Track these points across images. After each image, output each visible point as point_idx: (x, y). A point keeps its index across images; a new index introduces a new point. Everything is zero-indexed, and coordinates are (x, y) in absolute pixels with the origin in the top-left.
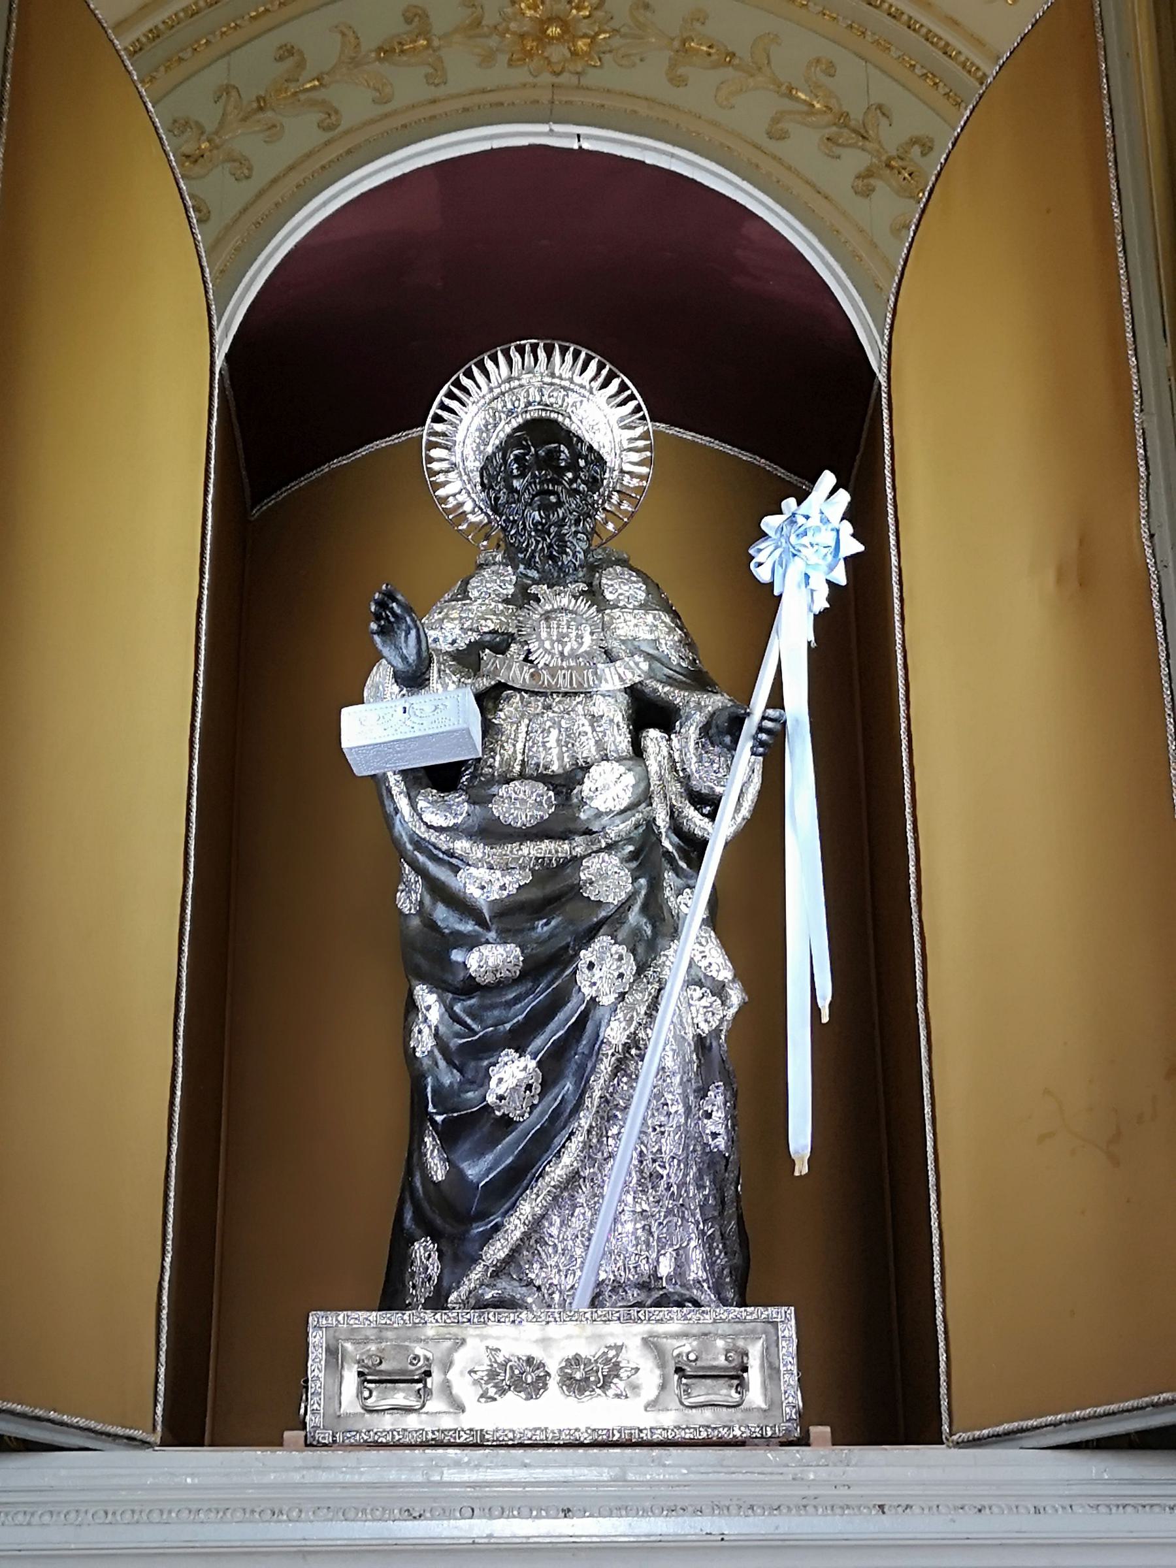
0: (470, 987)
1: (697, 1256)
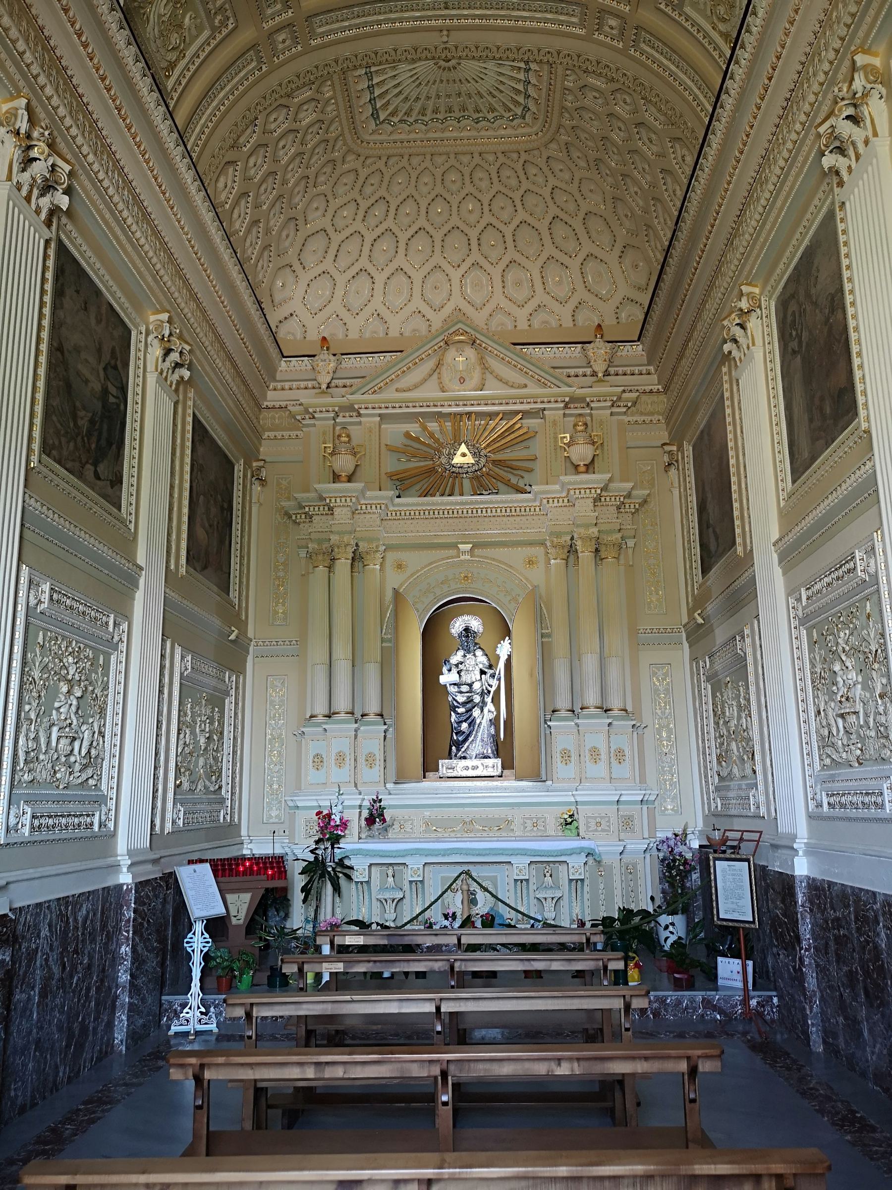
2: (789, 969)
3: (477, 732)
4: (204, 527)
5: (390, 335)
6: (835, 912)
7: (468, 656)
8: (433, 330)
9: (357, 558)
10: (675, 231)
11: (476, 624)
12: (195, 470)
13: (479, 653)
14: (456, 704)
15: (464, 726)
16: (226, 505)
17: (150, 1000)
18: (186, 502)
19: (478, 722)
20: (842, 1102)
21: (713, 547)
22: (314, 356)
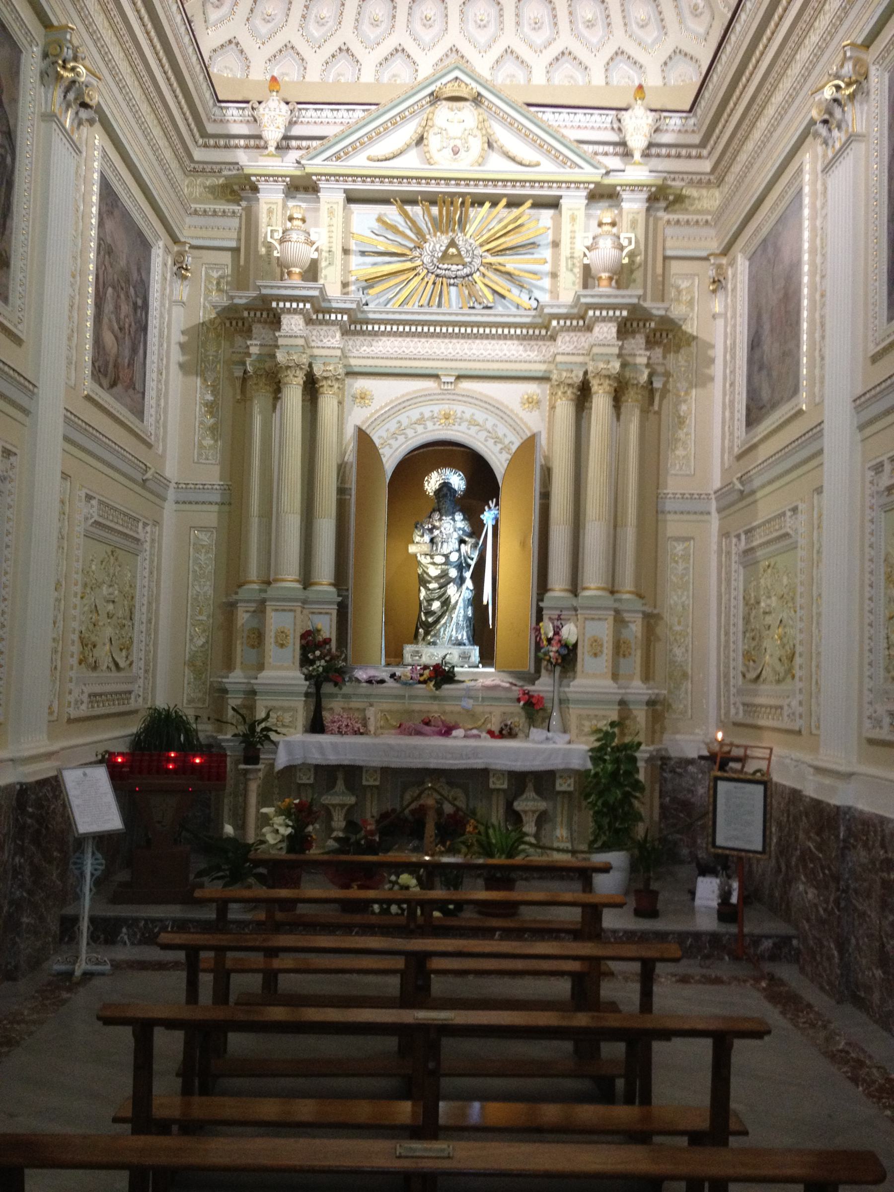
0: (429, 590)
1: (465, 634)
2: (817, 911)
4: (113, 332)
6: (886, 852)
8: (420, 79)
12: (102, 253)
15: (436, 605)
20: (879, 1068)
21: (765, 394)
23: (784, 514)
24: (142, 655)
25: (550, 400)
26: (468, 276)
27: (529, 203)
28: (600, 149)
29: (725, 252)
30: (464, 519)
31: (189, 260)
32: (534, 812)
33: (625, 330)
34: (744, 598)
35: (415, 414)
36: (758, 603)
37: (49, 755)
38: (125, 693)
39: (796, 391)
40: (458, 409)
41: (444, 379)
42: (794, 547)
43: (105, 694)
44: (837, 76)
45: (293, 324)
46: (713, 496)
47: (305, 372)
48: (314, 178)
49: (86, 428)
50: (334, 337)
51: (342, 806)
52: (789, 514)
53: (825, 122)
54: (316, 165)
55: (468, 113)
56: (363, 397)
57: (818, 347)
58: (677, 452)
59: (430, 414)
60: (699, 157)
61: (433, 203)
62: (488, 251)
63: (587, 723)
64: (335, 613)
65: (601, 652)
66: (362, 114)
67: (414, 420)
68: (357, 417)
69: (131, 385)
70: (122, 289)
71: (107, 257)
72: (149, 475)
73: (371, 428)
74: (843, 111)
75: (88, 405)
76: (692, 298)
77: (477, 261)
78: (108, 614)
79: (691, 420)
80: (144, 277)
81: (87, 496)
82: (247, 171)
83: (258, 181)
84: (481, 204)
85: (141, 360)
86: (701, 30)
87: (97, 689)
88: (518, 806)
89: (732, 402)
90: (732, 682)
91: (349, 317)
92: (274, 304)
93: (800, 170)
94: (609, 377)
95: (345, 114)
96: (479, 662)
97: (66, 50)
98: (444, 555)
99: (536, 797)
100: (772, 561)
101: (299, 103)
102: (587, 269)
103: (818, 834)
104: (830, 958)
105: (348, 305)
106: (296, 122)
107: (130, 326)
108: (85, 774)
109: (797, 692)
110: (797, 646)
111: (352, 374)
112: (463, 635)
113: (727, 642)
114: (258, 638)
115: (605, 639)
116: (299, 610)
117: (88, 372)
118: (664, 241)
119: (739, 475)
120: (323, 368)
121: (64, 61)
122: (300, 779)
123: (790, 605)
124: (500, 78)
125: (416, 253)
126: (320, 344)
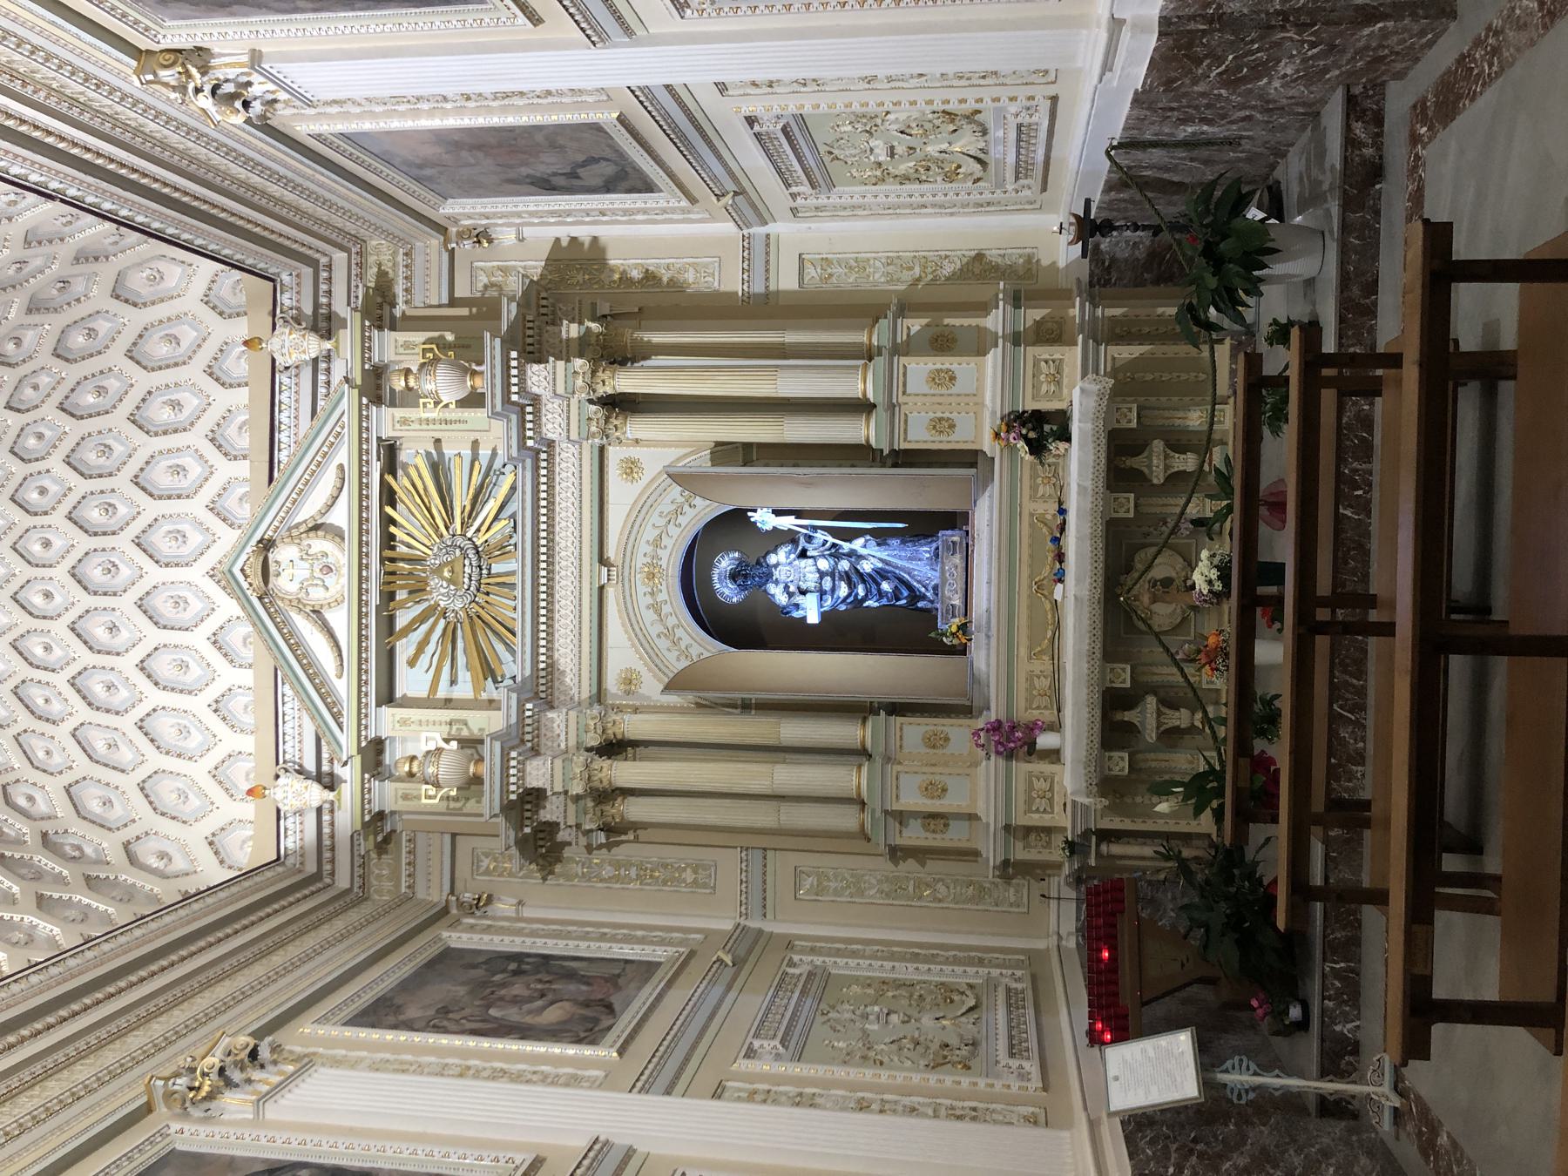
2: (1312, 57)
3: (897, 567)
4: (544, 1008)
5: (252, 685)
7: (776, 574)
8: (242, 614)
9: (614, 748)
10: (63, 201)
11: (725, 563)
13: (772, 559)
14: (851, 599)
15: (886, 586)
16: (513, 966)
17: (1326, 1140)
18: (500, 1045)
19: (880, 565)
21: (608, 169)
22: (278, 811)
23: (757, 136)
24: (959, 969)
25: (628, 446)
26: (478, 552)
27: (389, 478)
28: (322, 391)
29: (442, 230)
30: (775, 551)
31: (468, 897)
32: (1166, 457)
33: (535, 355)
34: (875, 184)
35: (649, 616)
36: (879, 164)
37: (1093, 1125)
38: (1008, 997)
39: (596, 128)
40: (640, 560)
41: (604, 580)
42: (801, 119)
43: (1010, 1028)
44: (182, 89)
45: (538, 774)
46: (746, 232)
47: (597, 757)
48: (363, 744)
49: (659, 1057)
50: (552, 720)
51: (1159, 713)
52: (757, 128)
53: (246, 105)
54: (348, 741)
55: (284, 554)
56: (629, 681)
57: (536, 101)
58: (691, 281)
59: (648, 596)
60: (329, 267)
61: (391, 596)
62: (447, 528)
63: (1044, 388)
64: (900, 719)
65: (948, 371)
66: (287, 687)
67: (656, 617)
68: (651, 688)
69: (613, 981)
70: (493, 993)
71: (451, 1016)
72: (728, 959)
73: (666, 671)
74: (227, 81)
75: (632, 1048)
76: (499, 268)
77: (459, 541)
78: (903, 1022)
79: (652, 265)
80: (481, 959)
81: (747, 1056)
82: (358, 826)
83: (370, 812)
84: (392, 537)
85: (584, 964)
86: (178, 270)
87: (1002, 1045)
88: (1158, 477)
89: (625, 212)
90: (987, 196)
91: (528, 700)
92: (513, 797)
93: (318, 137)
94: (594, 373)
95: (288, 706)
96: (961, 529)
97: (176, 1087)
98: (821, 578)
99: (1145, 454)
100: (823, 149)
101: (277, 763)
102: (463, 403)
103: (1199, 62)
104: (1385, 34)
105: (514, 703)
106: (301, 766)
107: (540, 981)
108: (1116, 1078)
109: (996, 104)
110: (935, 107)
111: (599, 696)
112: (925, 551)
113: (934, 205)
114: (934, 819)
115: (931, 366)
116: (897, 768)
117: (587, 1051)
118: (431, 306)
119: (714, 199)
120: (591, 734)
121: (191, 1089)
122: (1122, 769)
123: (879, 121)
124: (244, 512)
125: (451, 615)
126: (563, 737)
